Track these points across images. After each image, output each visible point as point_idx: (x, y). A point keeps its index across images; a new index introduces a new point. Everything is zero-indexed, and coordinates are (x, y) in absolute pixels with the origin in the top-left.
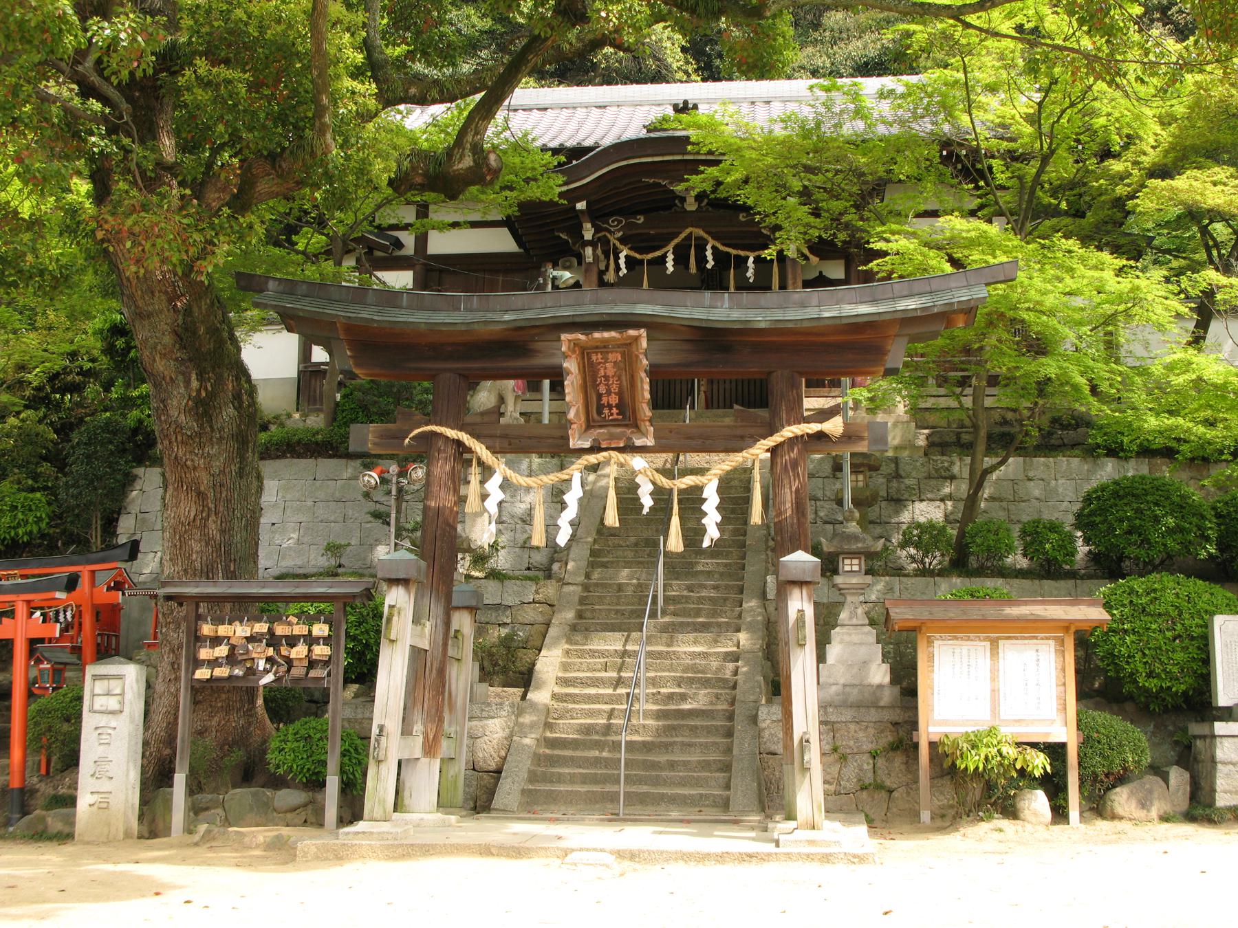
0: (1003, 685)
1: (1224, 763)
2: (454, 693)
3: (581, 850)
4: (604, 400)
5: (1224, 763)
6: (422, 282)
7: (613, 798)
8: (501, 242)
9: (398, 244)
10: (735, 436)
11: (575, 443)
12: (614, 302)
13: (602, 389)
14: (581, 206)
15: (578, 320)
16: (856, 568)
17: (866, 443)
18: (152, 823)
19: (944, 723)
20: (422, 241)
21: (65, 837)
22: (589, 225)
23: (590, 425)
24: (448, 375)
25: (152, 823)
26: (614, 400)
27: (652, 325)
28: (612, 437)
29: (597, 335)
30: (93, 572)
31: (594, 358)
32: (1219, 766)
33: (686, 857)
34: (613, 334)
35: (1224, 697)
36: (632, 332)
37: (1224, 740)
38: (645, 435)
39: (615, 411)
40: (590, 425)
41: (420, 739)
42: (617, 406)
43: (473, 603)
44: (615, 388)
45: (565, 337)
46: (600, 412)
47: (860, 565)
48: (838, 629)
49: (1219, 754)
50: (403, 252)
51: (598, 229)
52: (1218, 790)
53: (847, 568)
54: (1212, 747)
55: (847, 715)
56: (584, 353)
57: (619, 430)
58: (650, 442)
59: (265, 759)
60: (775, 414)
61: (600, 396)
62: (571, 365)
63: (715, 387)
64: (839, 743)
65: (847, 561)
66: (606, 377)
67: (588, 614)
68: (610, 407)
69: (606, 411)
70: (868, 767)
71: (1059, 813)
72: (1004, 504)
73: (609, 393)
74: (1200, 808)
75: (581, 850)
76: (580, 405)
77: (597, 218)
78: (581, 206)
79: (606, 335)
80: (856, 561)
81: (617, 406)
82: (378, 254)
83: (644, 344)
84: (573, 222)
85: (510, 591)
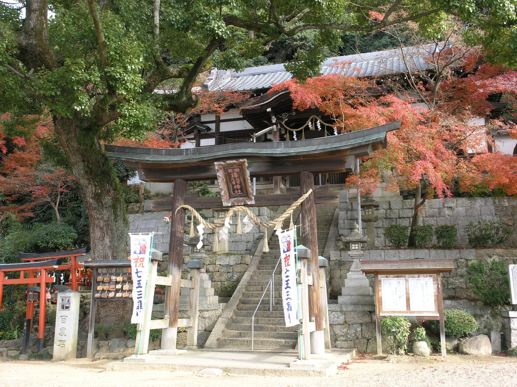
0: (411, 295)
1: (514, 330)
2: (191, 299)
3: (209, 367)
4: (235, 187)
5: (514, 330)
6: (219, 142)
7: (249, 343)
8: (245, 125)
9: (209, 129)
10: (287, 199)
11: (225, 204)
12: (240, 148)
13: (234, 183)
14: (269, 110)
15: (224, 156)
16: (357, 248)
17: (338, 199)
18: (81, 351)
19: (385, 312)
20: (218, 127)
21: (48, 357)
22: (274, 117)
23: (230, 197)
24: (179, 180)
25: (81, 351)
26: (238, 187)
27: (250, 157)
28: (239, 201)
29: (228, 162)
30: (75, 257)
31: (229, 171)
32: (512, 331)
33: (250, 371)
34: (234, 161)
35: (515, 301)
36: (241, 160)
37: (514, 319)
38: (251, 200)
39: (239, 191)
40: (230, 197)
41: (168, 320)
42: (240, 189)
43: (198, 266)
44: (238, 182)
45: (216, 163)
46: (234, 192)
47: (358, 246)
48: (350, 273)
49: (512, 326)
50: (211, 132)
51: (278, 119)
52: (512, 341)
53: (353, 248)
54: (509, 322)
55: (350, 308)
56: (225, 169)
57: (241, 198)
58: (253, 202)
59: (109, 329)
60: (302, 189)
61: (233, 185)
62: (220, 174)
63: (331, 176)
64: (347, 320)
65: (353, 245)
66: (235, 178)
67: (261, 268)
68: (237, 189)
69: (236, 191)
70: (359, 329)
71: (436, 349)
72: (435, 218)
73: (236, 184)
74: (505, 348)
75: (209, 367)
76: (226, 189)
77: (278, 114)
78: (269, 110)
79: (231, 162)
80: (357, 245)
81: (240, 189)
82: (202, 133)
83: (247, 165)
84: (268, 117)
85: (232, 260)
